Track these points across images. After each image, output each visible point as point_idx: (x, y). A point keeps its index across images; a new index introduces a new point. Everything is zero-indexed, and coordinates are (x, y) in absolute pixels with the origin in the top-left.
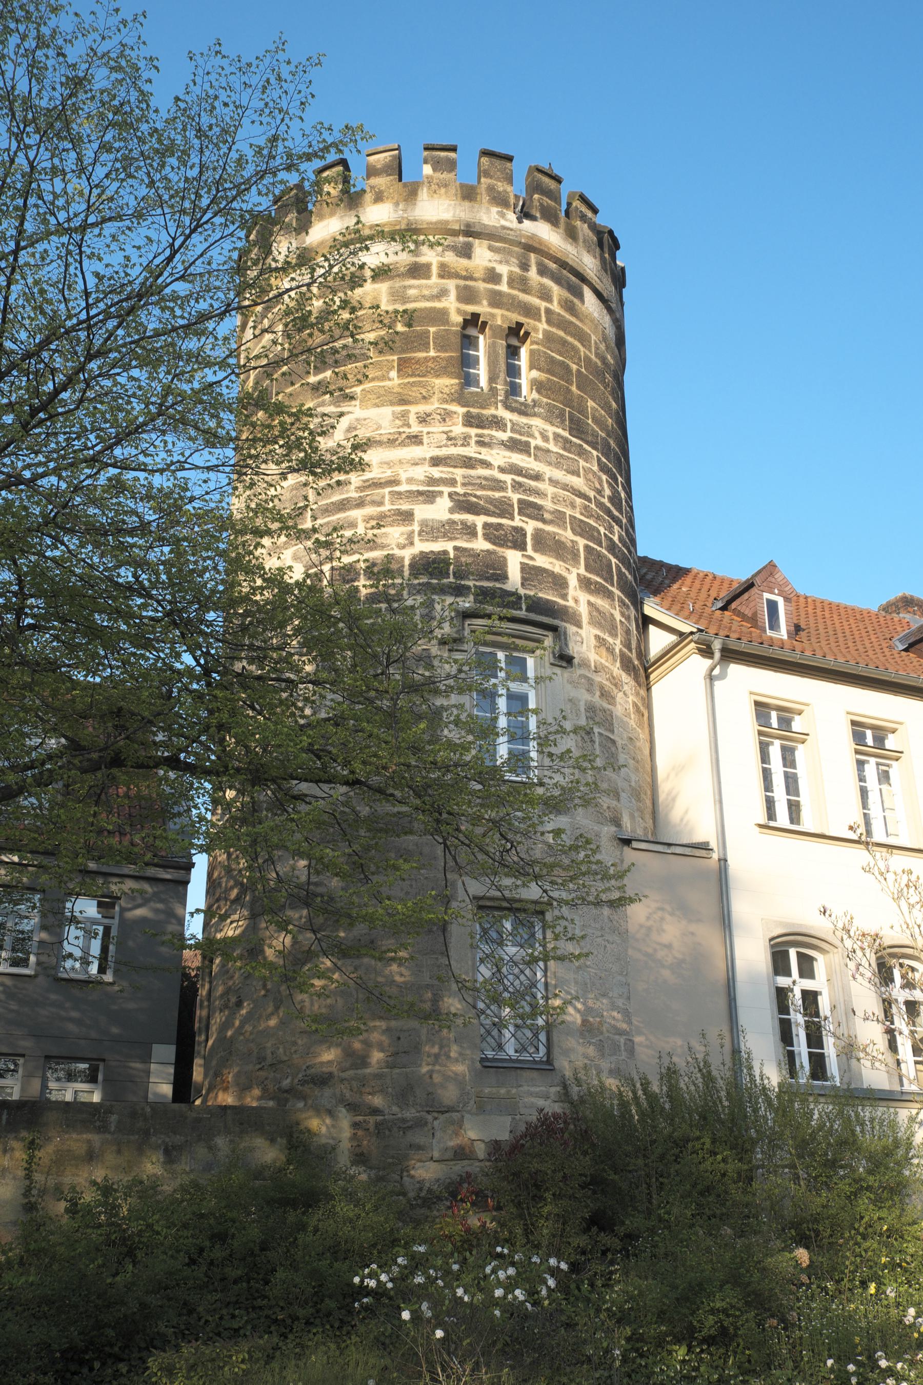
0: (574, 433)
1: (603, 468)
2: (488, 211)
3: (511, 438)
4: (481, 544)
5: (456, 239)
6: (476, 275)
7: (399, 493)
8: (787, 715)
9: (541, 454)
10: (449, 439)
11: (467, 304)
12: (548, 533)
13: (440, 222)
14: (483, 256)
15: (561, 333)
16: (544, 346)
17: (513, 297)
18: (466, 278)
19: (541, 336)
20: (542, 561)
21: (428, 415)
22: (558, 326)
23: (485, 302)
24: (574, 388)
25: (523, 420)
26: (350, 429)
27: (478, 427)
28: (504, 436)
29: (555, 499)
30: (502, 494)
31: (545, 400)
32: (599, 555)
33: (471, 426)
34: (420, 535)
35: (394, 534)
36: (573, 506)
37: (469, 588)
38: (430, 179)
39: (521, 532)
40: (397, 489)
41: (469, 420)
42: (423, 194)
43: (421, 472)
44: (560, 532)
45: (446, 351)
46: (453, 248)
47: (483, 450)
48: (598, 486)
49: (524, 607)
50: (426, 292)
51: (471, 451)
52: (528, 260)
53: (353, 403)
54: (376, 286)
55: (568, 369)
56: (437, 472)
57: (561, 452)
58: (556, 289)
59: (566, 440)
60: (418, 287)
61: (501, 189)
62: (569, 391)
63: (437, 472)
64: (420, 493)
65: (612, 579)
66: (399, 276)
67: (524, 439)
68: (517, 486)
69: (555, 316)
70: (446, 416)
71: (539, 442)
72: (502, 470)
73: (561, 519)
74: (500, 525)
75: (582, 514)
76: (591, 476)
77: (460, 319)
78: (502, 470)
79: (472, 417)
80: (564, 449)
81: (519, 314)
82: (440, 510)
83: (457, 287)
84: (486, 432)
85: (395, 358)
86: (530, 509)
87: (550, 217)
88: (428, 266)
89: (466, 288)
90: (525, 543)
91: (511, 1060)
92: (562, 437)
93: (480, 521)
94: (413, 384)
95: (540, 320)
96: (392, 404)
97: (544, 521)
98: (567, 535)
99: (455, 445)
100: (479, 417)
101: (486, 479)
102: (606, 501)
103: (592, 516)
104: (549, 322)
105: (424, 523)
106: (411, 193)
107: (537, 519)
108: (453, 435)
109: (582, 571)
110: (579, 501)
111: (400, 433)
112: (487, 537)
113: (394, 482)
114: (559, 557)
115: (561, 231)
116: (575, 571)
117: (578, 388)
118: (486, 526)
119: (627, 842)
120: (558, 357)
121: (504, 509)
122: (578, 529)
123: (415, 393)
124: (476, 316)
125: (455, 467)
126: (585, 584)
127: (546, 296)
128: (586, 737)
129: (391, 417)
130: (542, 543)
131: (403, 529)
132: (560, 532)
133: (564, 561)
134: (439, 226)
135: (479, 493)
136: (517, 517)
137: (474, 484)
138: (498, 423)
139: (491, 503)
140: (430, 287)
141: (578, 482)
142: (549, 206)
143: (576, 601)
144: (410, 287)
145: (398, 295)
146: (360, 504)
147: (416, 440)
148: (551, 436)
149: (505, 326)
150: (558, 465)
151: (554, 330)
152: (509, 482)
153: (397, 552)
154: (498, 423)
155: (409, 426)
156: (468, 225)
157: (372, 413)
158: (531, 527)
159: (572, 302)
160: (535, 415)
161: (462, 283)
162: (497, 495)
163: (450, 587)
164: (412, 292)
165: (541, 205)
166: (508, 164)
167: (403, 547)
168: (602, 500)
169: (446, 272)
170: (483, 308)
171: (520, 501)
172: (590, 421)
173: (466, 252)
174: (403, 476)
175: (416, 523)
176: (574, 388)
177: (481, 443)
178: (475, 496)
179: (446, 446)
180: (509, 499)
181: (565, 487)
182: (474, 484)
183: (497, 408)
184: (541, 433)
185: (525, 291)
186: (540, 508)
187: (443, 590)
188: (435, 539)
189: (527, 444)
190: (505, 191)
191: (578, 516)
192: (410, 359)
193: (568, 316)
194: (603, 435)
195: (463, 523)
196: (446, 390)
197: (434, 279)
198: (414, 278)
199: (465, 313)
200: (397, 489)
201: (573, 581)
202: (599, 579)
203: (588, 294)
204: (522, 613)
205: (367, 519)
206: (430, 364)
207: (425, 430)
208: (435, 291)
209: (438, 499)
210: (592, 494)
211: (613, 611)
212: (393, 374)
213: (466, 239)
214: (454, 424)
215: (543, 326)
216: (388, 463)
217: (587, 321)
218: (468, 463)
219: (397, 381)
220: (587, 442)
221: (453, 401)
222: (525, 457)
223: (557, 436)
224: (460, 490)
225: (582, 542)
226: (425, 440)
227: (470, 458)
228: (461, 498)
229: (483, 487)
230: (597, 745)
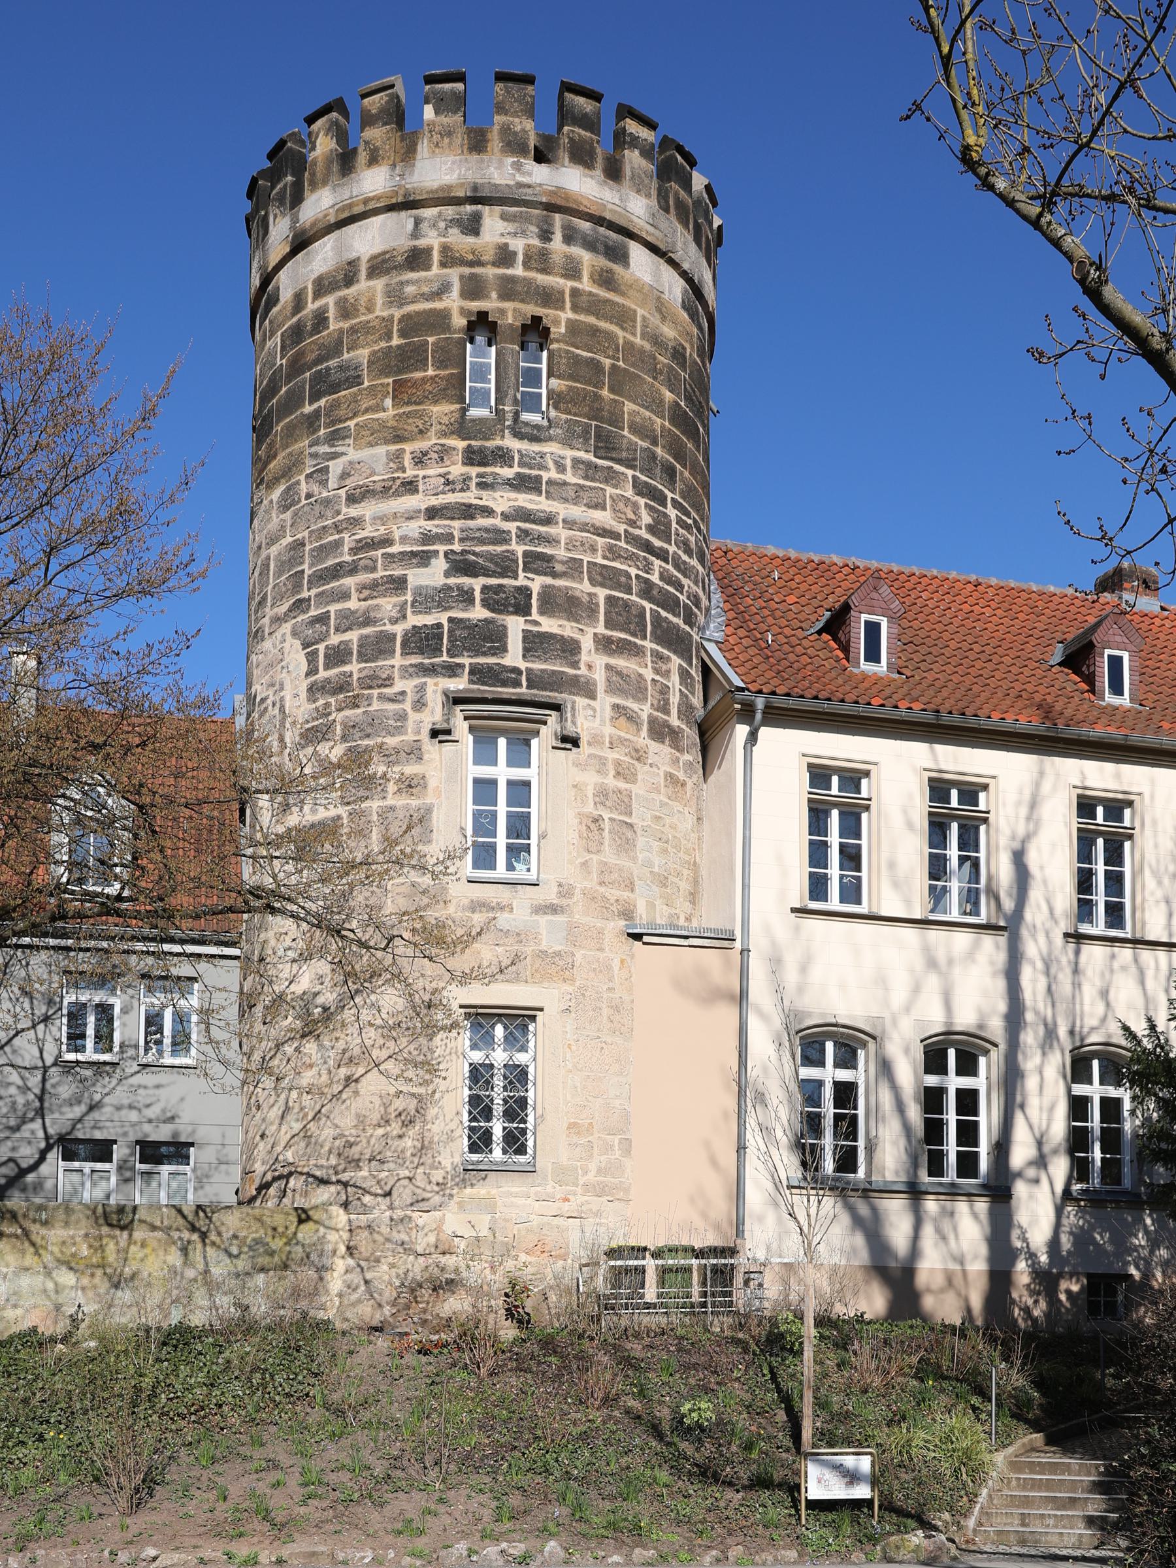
0: (602, 453)
1: (641, 489)
2: (501, 165)
3: (518, 474)
4: (479, 613)
5: (461, 208)
6: (485, 258)
7: (392, 556)
8: (853, 778)
9: (556, 489)
10: (448, 483)
11: (473, 300)
12: (559, 589)
13: (441, 189)
14: (494, 228)
15: (591, 320)
16: (567, 343)
17: (528, 282)
18: (471, 264)
19: (563, 330)
20: (549, 625)
21: (424, 454)
22: (588, 311)
23: (494, 295)
24: (605, 393)
25: (536, 448)
26: (345, 475)
27: (480, 464)
28: (508, 472)
29: (571, 545)
30: (504, 548)
31: (564, 416)
32: (627, 605)
33: (472, 464)
34: (413, 606)
35: (387, 605)
36: (593, 549)
37: (462, 666)
38: (432, 124)
39: (525, 592)
40: (390, 550)
41: (473, 457)
42: (423, 148)
43: (415, 528)
44: (574, 585)
45: (446, 367)
46: (457, 222)
47: (484, 494)
48: (631, 516)
49: (524, 683)
50: (426, 289)
51: (470, 497)
52: (552, 225)
53: (347, 441)
54: (371, 283)
55: (597, 367)
56: (434, 526)
57: (582, 482)
58: (586, 257)
59: (589, 465)
60: (417, 282)
61: (518, 128)
62: (597, 398)
63: (434, 526)
64: (414, 554)
65: (644, 630)
66: (395, 268)
67: (534, 472)
68: (523, 535)
69: (584, 298)
70: (444, 453)
71: (553, 474)
72: (506, 517)
73: (576, 570)
74: (501, 586)
75: (605, 557)
76: (621, 506)
77: (464, 322)
78: (506, 517)
79: (473, 452)
80: (586, 478)
81: (536, 304)
82: (434, 575)
83: (462, 277)
84: (488, 469)
85: (390, 380)
86: (538, 563)
87: (582, 156)
88: (428, 251)
89: (473, 276)
90: (529, 606)
91: (496, 1164)
92: (583, 462)
93: (477, 584)
94: (408, 415)
95: (562, 309)
96: (387, 442)
97: (555, 575)
98: (583, 587)
99: (453, 491)
100: (481, 451)
101: (487, 530)
102: (644, 534)
103: (620, 556)
104: (575, 308)
105: (418, 591)
106: (408, 153)
107: (546, 574)
108: (451, 477)
109: (601, 629)
110: (601, 541)
111: (394, 479)
112: (486, 604)
113: (387, 541)
114: (572, 617)
115: (598, 172)
116: (590, 631)
117: (612, 390)
118: (485, 589)
119: (637, 937)
120: (585, 354)
121: (506, 566)
122: (599, 579)
123: (411, 426)
124: (482, 315)
125: (452, 519)
126: (605, 645)
127: (572, 271)
128: (593, 826)
129: (385, 460)
130: (552, 602)
131: (395, 599)
132: (574, 585)
133: (578, 621)
134: (441, 195)
135: (477, 549)
136: (521, 574)
137: (473, 539)
138: (503, 456)
139: (491, 561)
140: (428, 281)
141: (603, 517)
142: (583, 141)
143: (590, 667)
144: (408, 282)
145: (395, 297)
146: (353, 570)
147: (410, 487)
148: (568, 463)
149: (518, 324)
150: (576, 501)
151: (582, 317)
152: (514, 531)
153: (389, 627)
154: (503, 456)
155: (404, 471)
156: (475, 188)
157: (365, 454)
158: (536, 584)
159: (610, 271)
160: (550, 439)
161: (467, 271)
162: (499, 549)
163: (443, 667)
164: (410, 290)
165: (571, 140)
166: (530, 88)
167: (394, 622)
168: (637, 532)
169: (450, 258)
170: (491, 304)
171: (526, 554)
172: (626, 433)
173: (473, 227)
174: (397, 535)
175: (409, 592)
176: (605, 393)
177: (482, 486)
178: (474, 554)
179: (444, 493)
180: (513, 552)
181: (584, 527)
182: (473, 539)
183: (503, 437)
184: (556, 463)
185: (545, 271)
186: (549, 559)
187: (431, 671)
188: (428, 611)
189: (538, 479)
190: (523, 130)
191: (600, 561)
192: (406, 381)
193: (603, 293)
194: (645, 444)
195: (459, 588)
196: (445, 420)
197: (435, 269)
198: (413, 270)
199: (470, 313)
200: (390, 550)
201: (587, 643)
202: (623, 636)
203: (637, 252)
204: (523, 691)
205: (361, 588)
206: (427, 387)
207: (421, 473)
208: (435, 287)
209: (433, 561)
210: (621, 528)
211: (642, 671)
212: (388, 402)
213: (474, 207)
214: (454, 464)
215: (567, 314)
216: (381, 518)
217: (631, 292)
218: (468, 511)
219: (391, 412)
220: (619, 461)
221: (453, 433)
222: (533, 497)
223: (576, 462)
224: (457, 547)
225: (602, 593)
226: (421, 488)
227: (470, 506)
228: (458, 558)
229: (483, 542)
230: (606, 833)
